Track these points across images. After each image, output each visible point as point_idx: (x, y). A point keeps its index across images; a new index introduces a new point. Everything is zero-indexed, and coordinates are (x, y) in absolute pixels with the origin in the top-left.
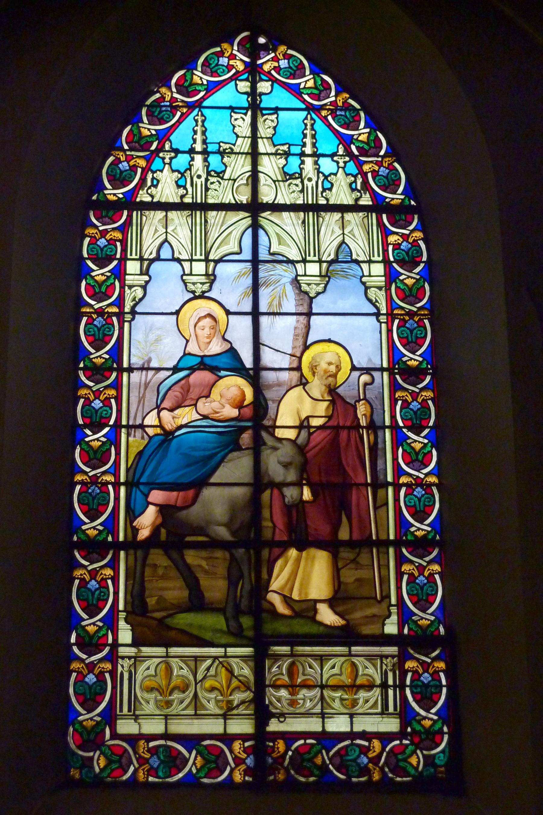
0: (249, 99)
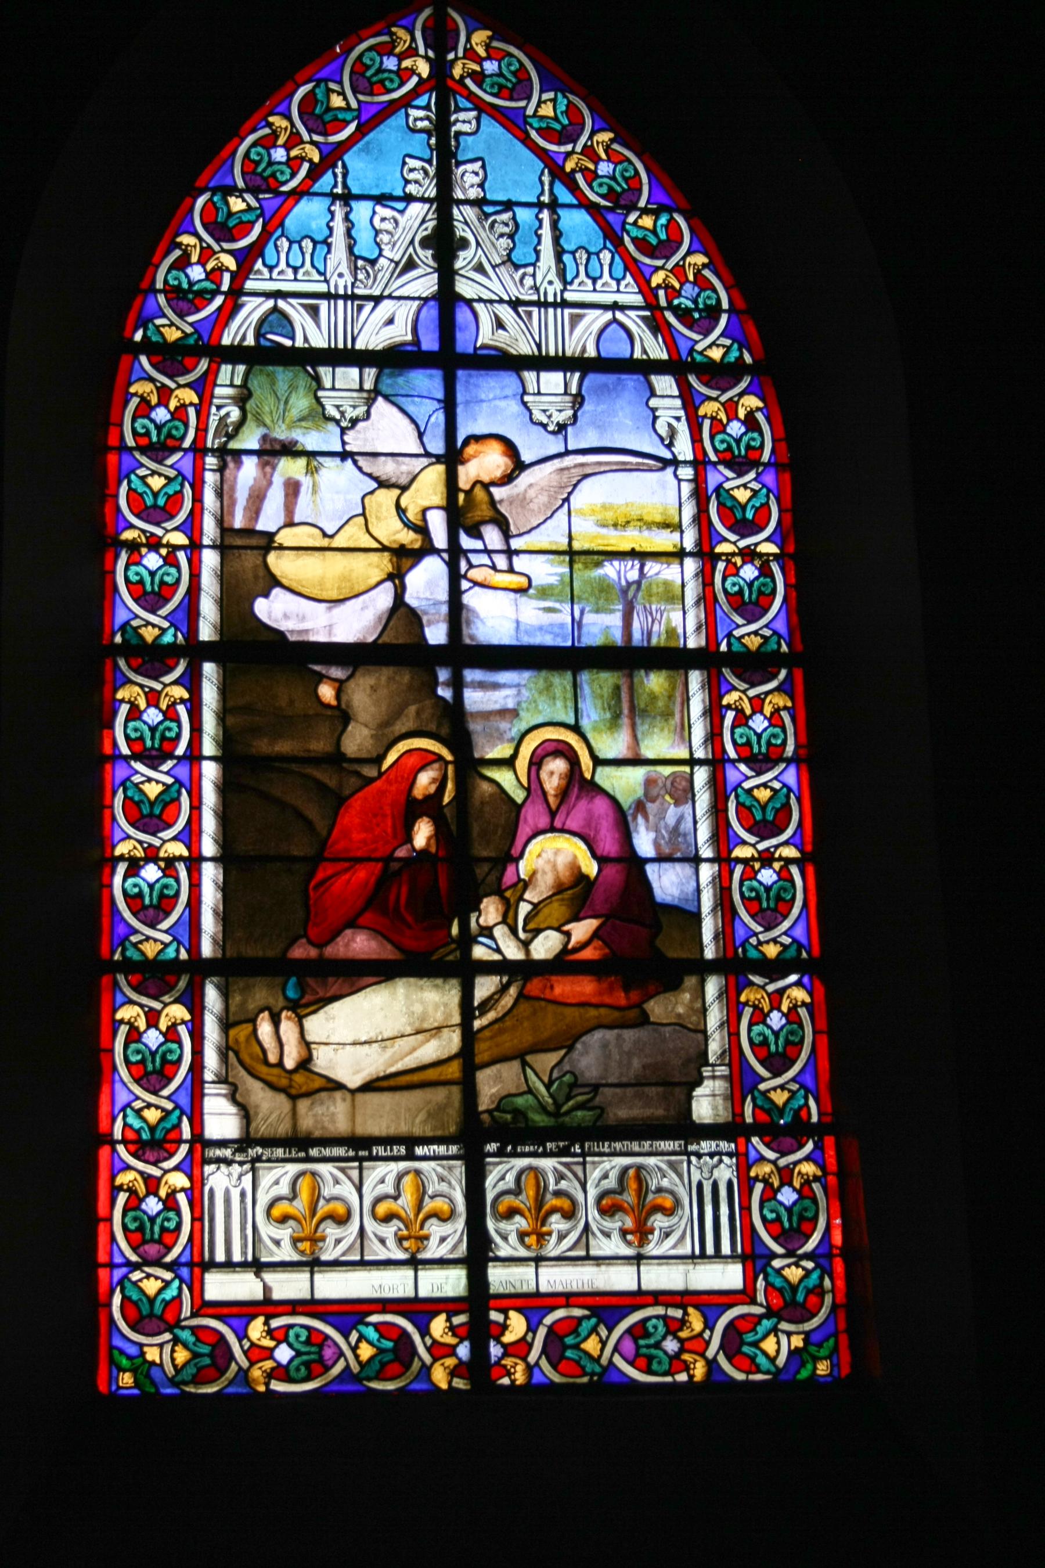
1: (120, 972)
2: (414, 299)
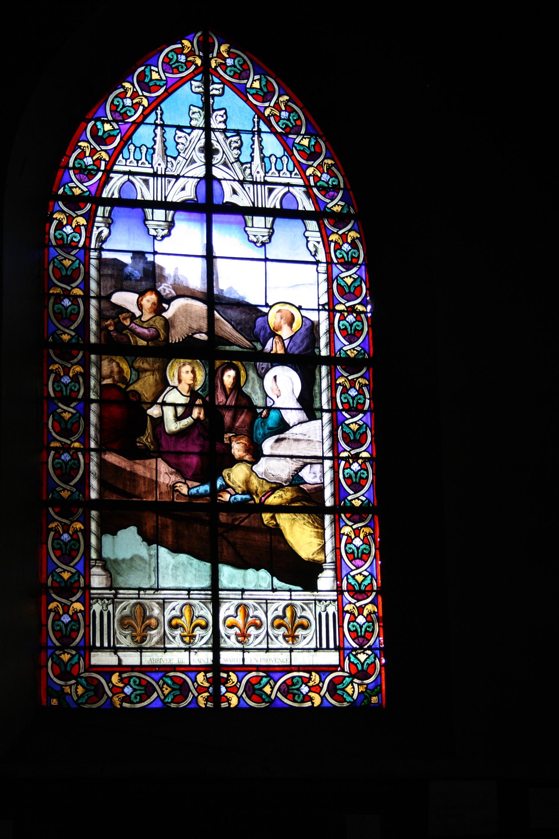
0: (203, 99)
2: (195, 178)
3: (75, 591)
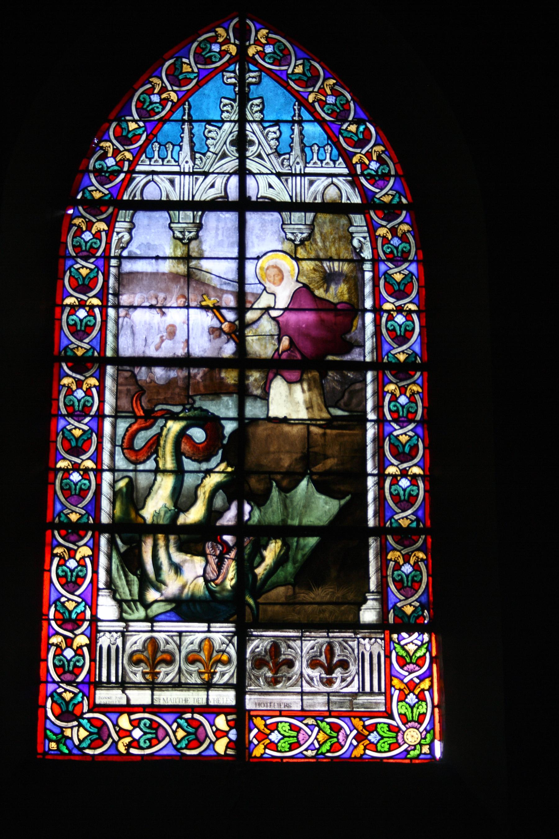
1: (63, 362)
3: (80, 623)
